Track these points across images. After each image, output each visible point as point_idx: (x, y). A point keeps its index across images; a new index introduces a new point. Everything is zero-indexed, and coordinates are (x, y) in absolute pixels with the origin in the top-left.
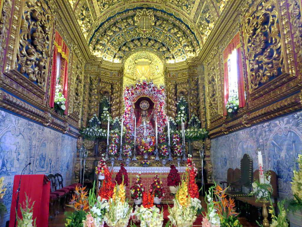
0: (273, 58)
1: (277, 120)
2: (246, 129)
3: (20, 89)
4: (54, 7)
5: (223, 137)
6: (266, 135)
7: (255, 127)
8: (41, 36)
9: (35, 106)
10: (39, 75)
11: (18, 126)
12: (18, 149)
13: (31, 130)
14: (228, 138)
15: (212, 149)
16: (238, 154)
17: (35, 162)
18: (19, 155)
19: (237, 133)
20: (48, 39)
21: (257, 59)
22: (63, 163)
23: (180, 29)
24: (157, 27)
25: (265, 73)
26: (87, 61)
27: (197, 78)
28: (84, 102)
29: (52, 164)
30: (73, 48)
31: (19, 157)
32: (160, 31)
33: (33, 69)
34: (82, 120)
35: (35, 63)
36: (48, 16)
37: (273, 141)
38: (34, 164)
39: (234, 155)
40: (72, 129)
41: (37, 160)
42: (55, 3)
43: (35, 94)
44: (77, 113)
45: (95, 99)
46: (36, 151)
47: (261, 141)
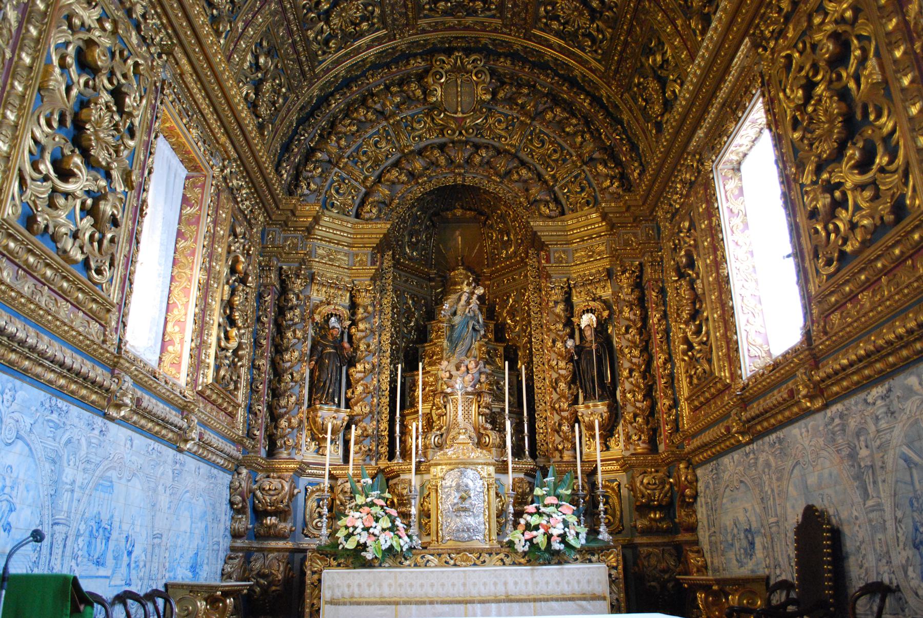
0: (874, 167)
1: (911, 374)
2: (812, 417)
3: (27, 287)
4: (162, 39)
5: (736, 455)
6: (878, 431)
7: (838, 407)
8: (107, 119)
9: (78, 348)
10: (96, 244)
11: (11, 409)
12: (7, 490)
13: (57, 427)
14: (752, 456)
15: (701, 500)
16: (789, 510)
17: (69, 543)
18: (11, 510)
19: (780, 434)
20: (132, 133)
21: (825, 176)
22: (177, 556)
23: (569, 107)
24: (499, 108)
25: (855, 219)
26: (269, 215)
27: (640, 264)
28: (259, 352)
29: (133, 555)
30: (222, 171)
31: (12, 518)
32: (510, 118)
33: (76, 225)
34: (249, 409)
35: (83, 203)
36: (136, 65)
37: (905, 449)
38: (68, 548)
39: (776, 516)
40: (210, 436)
41: (78, 535)
42: (166, 29)
43: (77, 305)
44: (229, 384)
45: (296, 340)
46: (75, 503)
47: (864, 453)
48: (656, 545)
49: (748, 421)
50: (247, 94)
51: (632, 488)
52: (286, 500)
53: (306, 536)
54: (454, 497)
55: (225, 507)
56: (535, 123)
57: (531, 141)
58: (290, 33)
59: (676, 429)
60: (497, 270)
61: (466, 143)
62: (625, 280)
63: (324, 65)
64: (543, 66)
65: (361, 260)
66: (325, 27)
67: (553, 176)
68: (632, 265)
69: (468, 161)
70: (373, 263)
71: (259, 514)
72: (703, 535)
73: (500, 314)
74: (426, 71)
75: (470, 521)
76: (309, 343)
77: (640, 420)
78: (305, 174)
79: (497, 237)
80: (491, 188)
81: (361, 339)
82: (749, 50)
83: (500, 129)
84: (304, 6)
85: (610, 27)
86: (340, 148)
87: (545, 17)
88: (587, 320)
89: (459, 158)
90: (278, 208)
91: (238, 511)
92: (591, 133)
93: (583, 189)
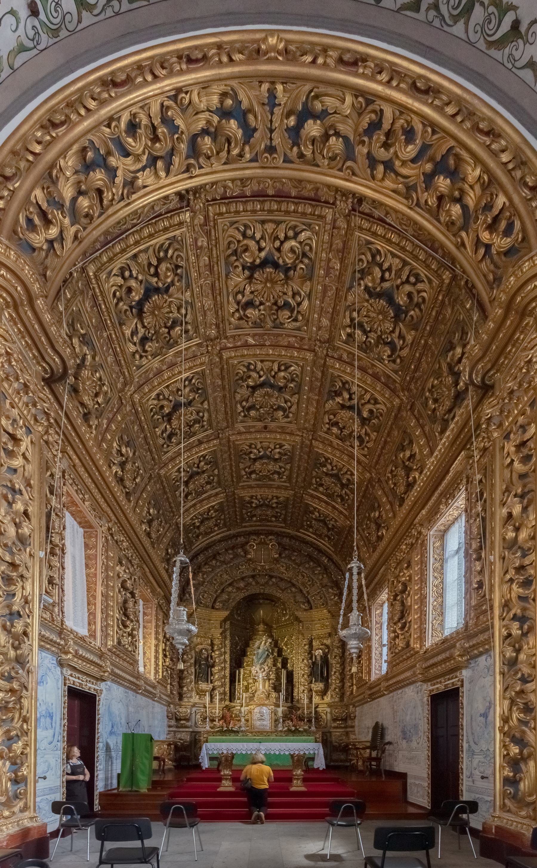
5: (368, 704)
24: (283, 560)
49: (426, 668)
50: (116, 472)
51: (331, 713)
54: (258, 715)
55: (166, 717)
56: (300, 568)
57: (298, 576)
58: (142, 429)
59: (352, 693)
61: (266, 575)
63: (169, 454)
64: (306, 543)
66: (168, 426)
67: (308, 592)
69: (267, 583)
70: (221, 627)
71: (178, 720)
72: (356, 729)
74: (247, 543)
75: (265, 723)
76: (193, 659)
80: (278, 595)
82: (463, 460)
83: (282, 569)
84: (174, 479)
85: (375, 431)
86: (203, 578)
87: (328, 424)
88: (318, 653)
89: (262, 581)
91: (170, 719)
92: (327, 574)
93: (321, 598)
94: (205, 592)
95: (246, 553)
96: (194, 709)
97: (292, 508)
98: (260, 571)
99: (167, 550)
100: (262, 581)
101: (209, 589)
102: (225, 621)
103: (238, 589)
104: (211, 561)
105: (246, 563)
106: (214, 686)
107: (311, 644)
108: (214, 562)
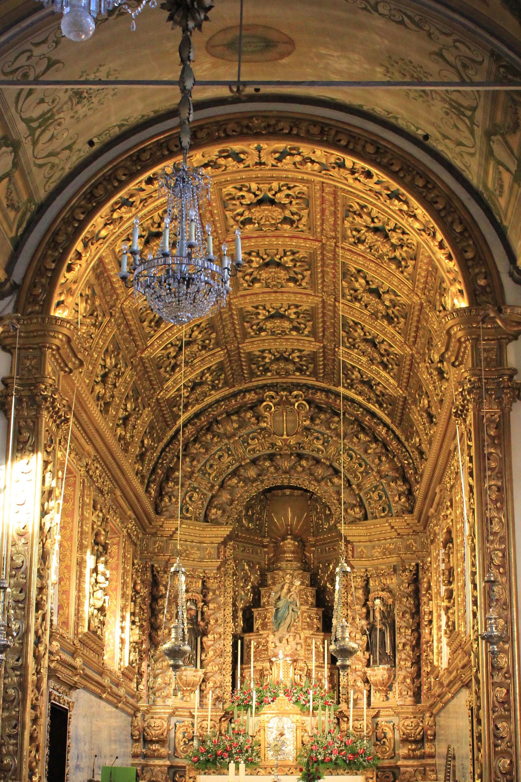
24: (316, 428)
48: (413, 766)
52: (165, 733)
53: (176, 757)
60: (321, 540)
61: (292, 454)
62: (406, 576)
65: (210, 553)
68: (410, 565)
71: (147, 742)
73: (322, 577)
77: (408, 681)
78: (167, 490)
79: (321, 510)
81: (210, 615)
89: (286, 464)
90: (151, 524)
94: (195, 489)
95: (259, 418)
96: (173, 720)
97: (323, 360)
98: (281, 449)
99: (142, 442)
100: (286, 464)
101: (200, 483)
102: (224, 543)
103: (247, 481)
104: (205, 435)
105: (260, 433)
106: (205, 674)
107: (367, 591)
108: (209, 437)
